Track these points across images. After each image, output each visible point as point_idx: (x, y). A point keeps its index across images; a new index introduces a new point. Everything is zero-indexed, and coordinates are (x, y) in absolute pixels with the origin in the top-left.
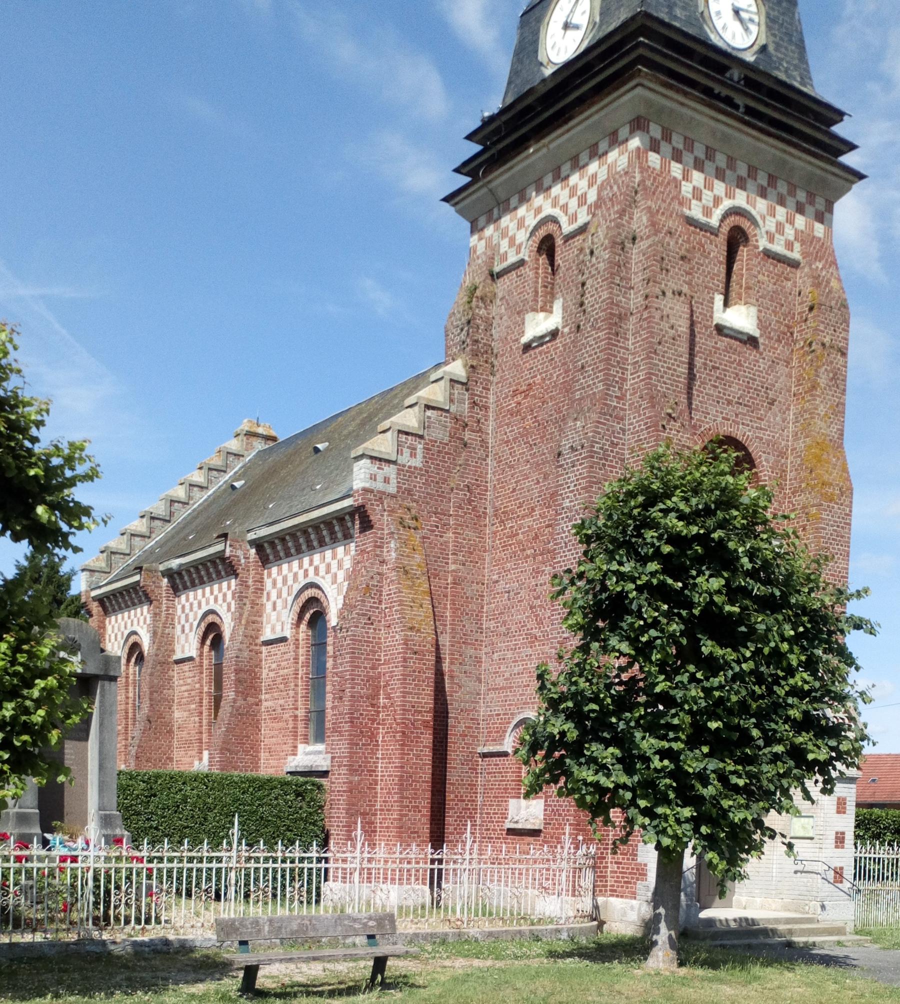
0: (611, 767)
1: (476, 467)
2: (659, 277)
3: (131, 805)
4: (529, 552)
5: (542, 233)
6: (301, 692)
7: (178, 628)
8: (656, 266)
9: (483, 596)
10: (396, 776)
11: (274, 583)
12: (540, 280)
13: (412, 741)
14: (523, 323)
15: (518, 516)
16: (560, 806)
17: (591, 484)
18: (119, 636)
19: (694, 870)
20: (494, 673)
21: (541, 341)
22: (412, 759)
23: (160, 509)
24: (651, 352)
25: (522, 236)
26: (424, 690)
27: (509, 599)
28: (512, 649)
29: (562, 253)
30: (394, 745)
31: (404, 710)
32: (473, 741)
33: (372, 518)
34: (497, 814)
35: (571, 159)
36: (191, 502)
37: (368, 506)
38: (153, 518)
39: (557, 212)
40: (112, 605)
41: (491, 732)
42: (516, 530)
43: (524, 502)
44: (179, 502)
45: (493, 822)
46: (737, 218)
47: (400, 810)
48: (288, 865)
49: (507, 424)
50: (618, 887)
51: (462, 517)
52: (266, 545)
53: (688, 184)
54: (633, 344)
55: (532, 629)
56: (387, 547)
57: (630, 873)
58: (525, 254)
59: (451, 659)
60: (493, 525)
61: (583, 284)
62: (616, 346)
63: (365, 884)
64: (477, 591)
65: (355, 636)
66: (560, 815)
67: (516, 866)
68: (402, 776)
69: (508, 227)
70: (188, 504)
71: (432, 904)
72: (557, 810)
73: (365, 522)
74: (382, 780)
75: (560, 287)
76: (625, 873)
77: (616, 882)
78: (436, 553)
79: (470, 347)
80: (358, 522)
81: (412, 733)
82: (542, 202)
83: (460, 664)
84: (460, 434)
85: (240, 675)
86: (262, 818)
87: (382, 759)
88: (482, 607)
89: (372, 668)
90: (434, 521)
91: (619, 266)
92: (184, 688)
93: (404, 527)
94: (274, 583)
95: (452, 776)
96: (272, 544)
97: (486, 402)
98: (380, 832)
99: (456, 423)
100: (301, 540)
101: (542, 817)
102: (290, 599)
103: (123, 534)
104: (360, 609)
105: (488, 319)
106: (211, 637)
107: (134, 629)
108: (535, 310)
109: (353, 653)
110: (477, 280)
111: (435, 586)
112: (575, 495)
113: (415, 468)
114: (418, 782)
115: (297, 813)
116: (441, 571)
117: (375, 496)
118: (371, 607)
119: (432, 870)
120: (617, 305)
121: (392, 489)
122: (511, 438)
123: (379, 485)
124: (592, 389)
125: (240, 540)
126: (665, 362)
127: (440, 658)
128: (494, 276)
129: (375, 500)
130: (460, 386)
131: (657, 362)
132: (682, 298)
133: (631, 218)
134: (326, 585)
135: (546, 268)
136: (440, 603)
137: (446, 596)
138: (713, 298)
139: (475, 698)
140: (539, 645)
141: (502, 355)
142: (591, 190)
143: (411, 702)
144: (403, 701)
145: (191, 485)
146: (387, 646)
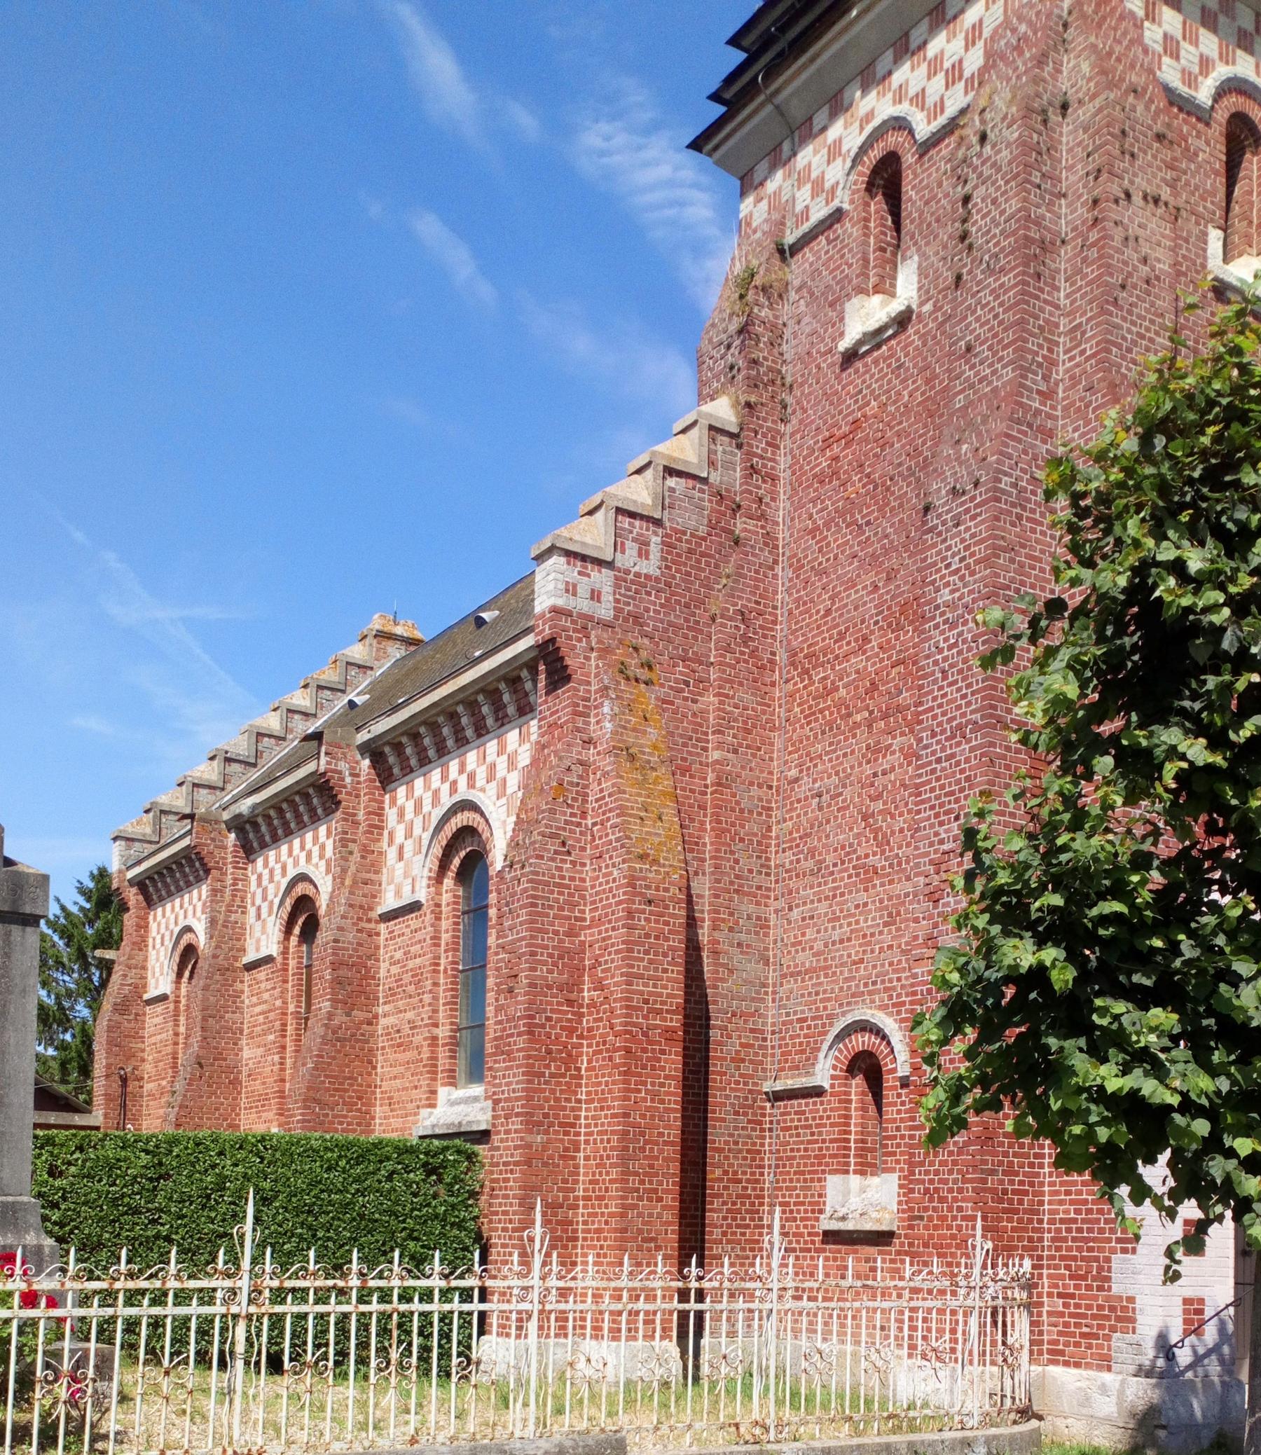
0: (1162, 1056)
1: (756, 580)
2: (1120, 165)
3: (123, 1196)
4: (858, 718)
5: (876, 154)
6: (443, 996)
7: (252, 911)
8: (1113, 145)
9: (770, 809)
10: (613, 1132)
11: (401, 814)
12: (872, 240)
13: (644, 1067)
14: (842, 319)
15: (837, 657)
16: (940, 1181)
17: (996, 551)
18: (167, 938)
19: (1231, 1310)
20: (793, 945)
21: (878, 339)
22: (645, 1100)
23: (241, 746)
24: (1107, 302)
25: (836, 172)
26: (665, 971)
27: (820, 808)
28: (827, 898)
29: (916, 176)
30: (610, 1075)
31: (628, 1007)
32: (755, 1070)
33: (568, 661)
34: (803, 1204)
35: (930, 14)
36: (290, 737)
37: (561, 641)
38: (228, 760)
39: (903, 109)
40: (158, 890)
41: (789, 1053)
42: (833, 683)
43: (847, 629)
44: (270, 736)
45: (795, 1219)
46: (1241, 99)
47: (622, 1198)
48: (374, 1307)
49: (813, 501)
50: (1067, 1344)
51: (733, 667)
52: (387, 749)
53: (1154, 27)
54: (1067, 296)
55: (867, 856)
56: (597, 715)
57: (1094, 1317)
58: (843, 200)
59: (714, 920)
60: (787, 681)
61: (966, 199)
62: (1037, 298)
63: (552, 1341)
64: (760, 800)
65: (537, 873)
66: (942, 1200)
67: (876, 1304)
68: (626, 1133)
69: (810, 165)
70: (284, 739)
71: (685, 1377)
72: (936, 1190)
73: (556, 671)
74: (587, 1142)
75: (912, 237)
76: (1084, 1316)
77: (1060, 1333)
78: (685, 729)
79: (743, 373)
80: (542, 677)
81: (644, 1050)
82: (874, 103)
83: (731, 929)
84: (728, 523)
85: (341, 973)
86: (362, 1216)
87: (587, 1102)
88: (769, 829)
89: (568, 934)
90: (681, 673)
91: (1040, 153)
92: (258, 1009)
93: (628, 679)
94: (401, 814)
95: (718, 1135)
96: (398, 748)
97: (773, 468)
98: (585, 1239)
99: (719, 503)
100: (446, 731)
101: (895, 1208)
102: (426, 836)
103: (180, 785)
104: (547, 826)
105: (774, 325)
106: (300, 922)
107: (187, 923)
108: (861, 291)
109: (534, 905)
110: (755, 263)
111: (683, 789)
112: (962, 578)
113: (647, 577)
114: (657, 1143)
115: (428, 1205)
116: (694, 762)
117: (573, 622)
118: (566, 822)
119: (683, 1315)
120: (1038, 224)
121: (605, 611)
122: (820, 522)
123: (582, 604)
124: (990, 383)
125: (343, 744)
126: (1133, 323)
127: (694, 918)
128: (785, 253)
129: (575, 630)
130: (726, 439)
131: (1118, 321)
132: (1161, 211)
133: (1059, 71)
134: (487, 802)
135: (882, 218)
136: (692, 820)
137: (702, 807)
138: (1206, 234)
139: (758, 993)
140: (882, 885)
141: (802, 385)
142: (972, 51)
143: (642, 993)
144: (628, 991)
145: (289, 711)
146: (597, 893)
